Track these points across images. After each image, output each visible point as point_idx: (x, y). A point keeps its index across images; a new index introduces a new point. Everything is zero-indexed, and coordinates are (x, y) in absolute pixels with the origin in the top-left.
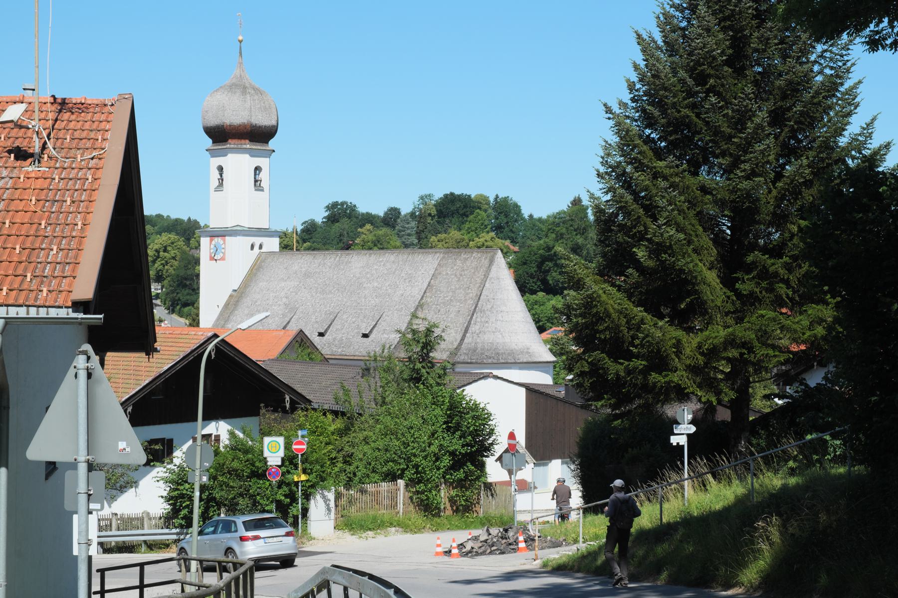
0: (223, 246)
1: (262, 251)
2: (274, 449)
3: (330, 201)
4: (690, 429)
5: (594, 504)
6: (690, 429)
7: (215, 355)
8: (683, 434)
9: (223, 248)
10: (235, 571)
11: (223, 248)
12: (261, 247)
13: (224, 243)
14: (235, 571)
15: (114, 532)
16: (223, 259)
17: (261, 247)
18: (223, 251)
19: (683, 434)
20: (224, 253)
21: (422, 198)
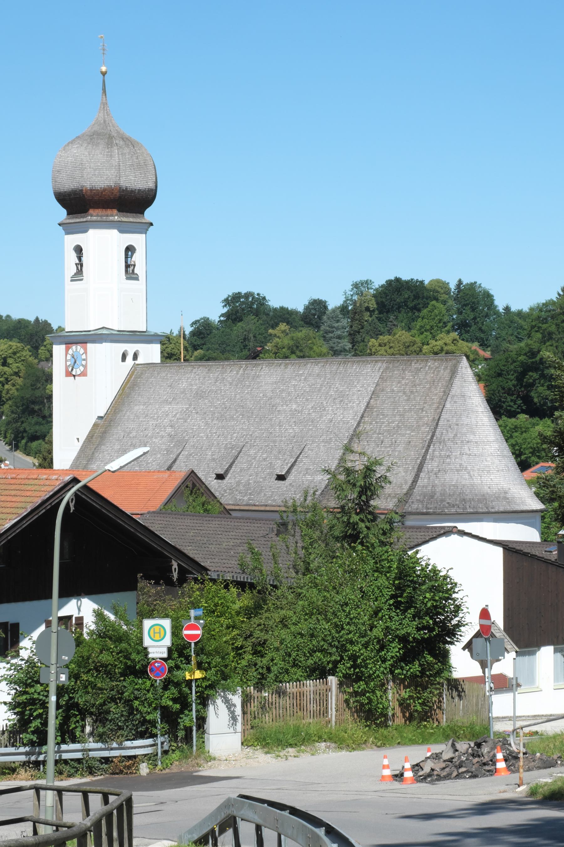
0: (84, 357)
1: (137, 362)
3: (229, 291)
9: (84, 360)
11: (84, 360)
12: (135, 357)
13: (86, 352)
16: (84, 374)
17: (135, 357)
18: (84, 363)
20: (85, 367)
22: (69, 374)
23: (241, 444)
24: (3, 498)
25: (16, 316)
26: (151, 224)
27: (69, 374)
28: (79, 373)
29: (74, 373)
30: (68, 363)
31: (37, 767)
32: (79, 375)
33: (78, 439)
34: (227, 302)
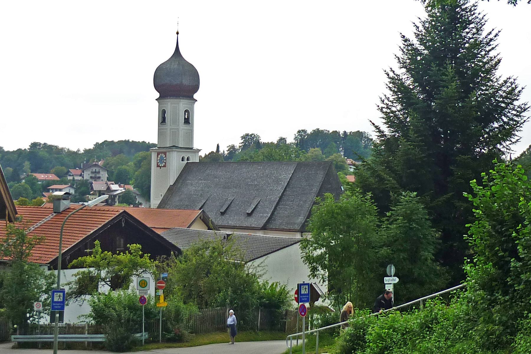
0: (165, 159)
1: (188, 162)
2: (143, 285)
3: (243, 133)
4: (395, 280)
5: (144, 314)
6: (395, 280)
7: (125, 224)
8: (391, 284)
9: (165, 160)
10: (311, 330)
11: (165, 160)
12: (188, 159)
13: (166, 157)
14: (311, 330)
15: (86, 335)
16: (165, 166)
17: (188, 159)
18: (165, 161)
19: (391, 284)
20: (165, 163)
21: (299, 132)
22: (158, 166)
23: (232, 199)
24: (1, 232)
25: (60, 146)
26: (197, 101)
27: (158, 166)
28: (162, 166)
29: (161, 166)
30: (158, 161)
31: (356, 326)
32: (163, 167)
33: (161, 195)
34: (243, 138)
